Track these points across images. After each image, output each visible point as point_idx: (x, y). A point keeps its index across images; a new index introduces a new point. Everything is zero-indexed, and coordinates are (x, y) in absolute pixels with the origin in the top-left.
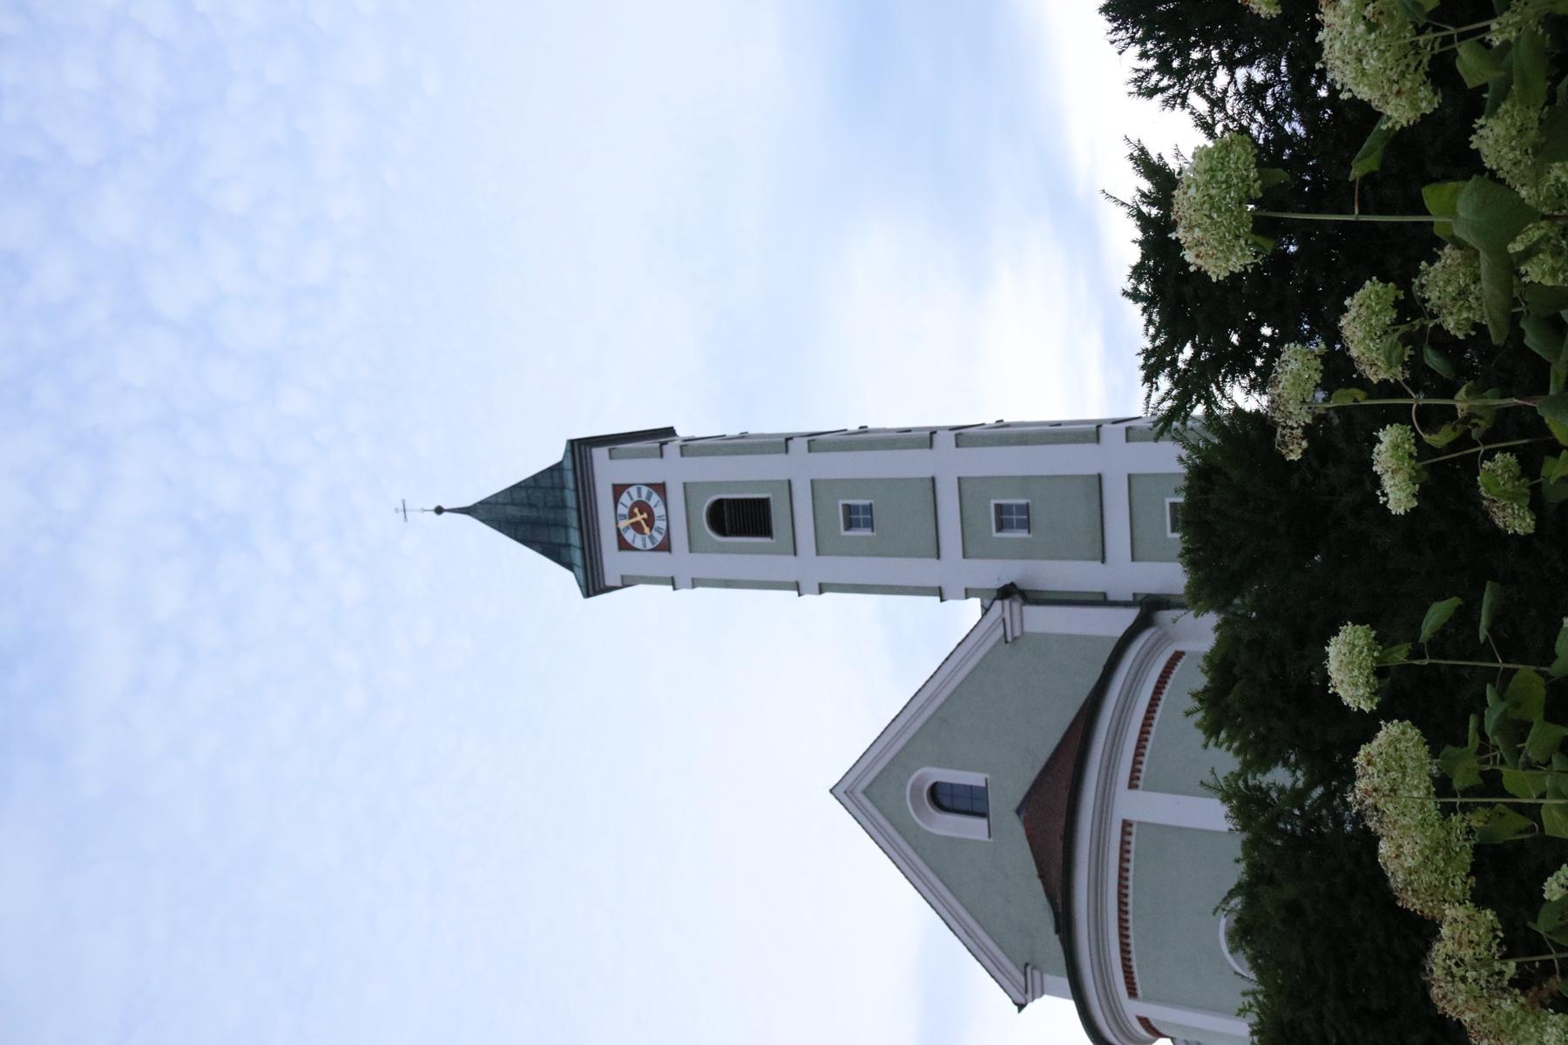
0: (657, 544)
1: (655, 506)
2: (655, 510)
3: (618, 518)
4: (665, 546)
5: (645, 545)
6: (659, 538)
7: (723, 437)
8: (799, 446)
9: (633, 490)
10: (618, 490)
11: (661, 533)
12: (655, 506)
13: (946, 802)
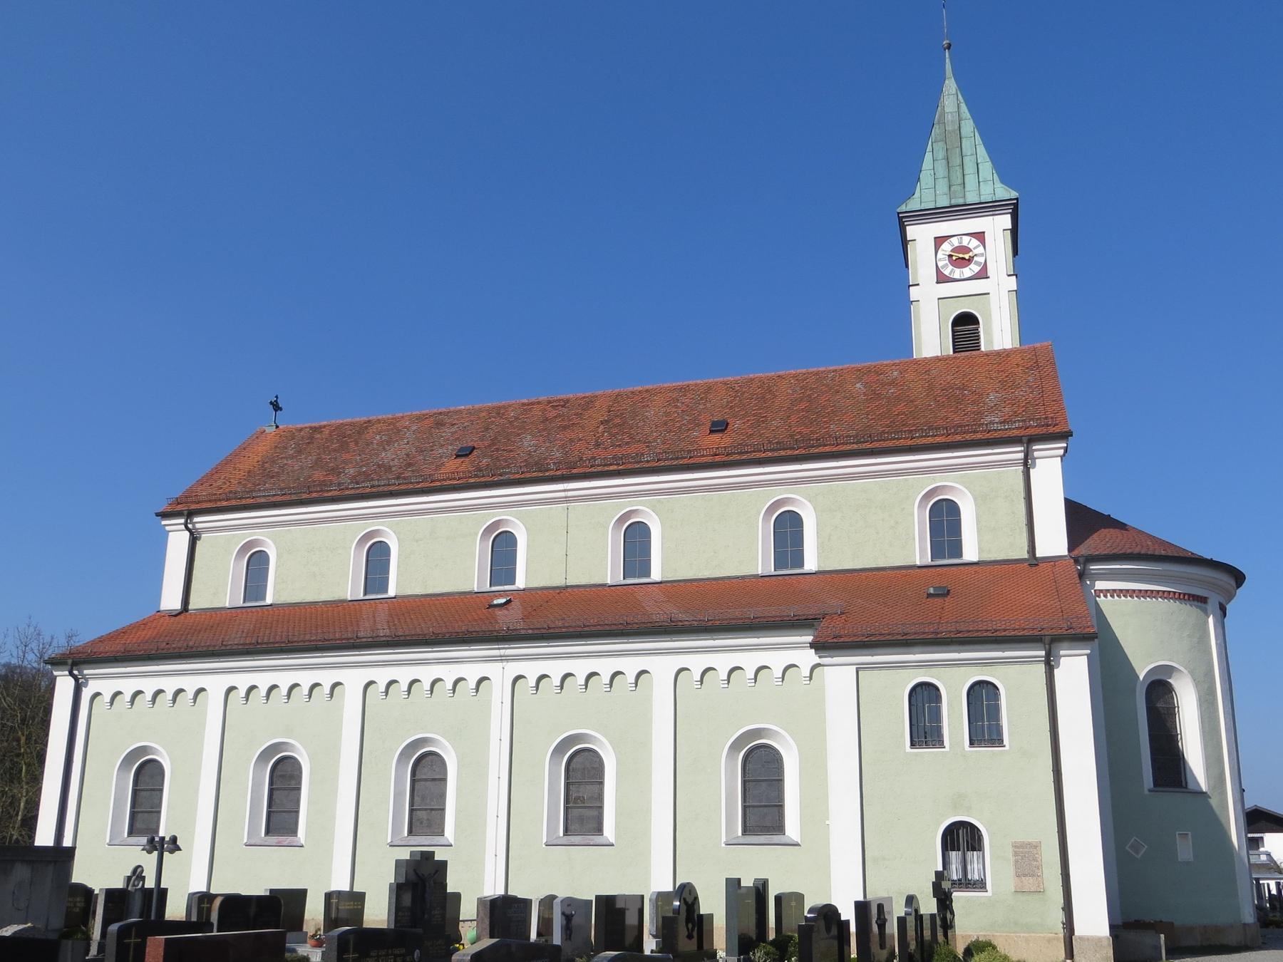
0: (942, 270)
1: (970, 269)
2: (967, 269)
3: (959, 237)
4: (942, 279)
5: (940, 260)
6: (947, 272)
7: (1054, 781)
8: (1143, 592)
9: (981, 250)
10: (980, 236)
11: (950, 274)
12: (970, 269)
13: (424, 773)
